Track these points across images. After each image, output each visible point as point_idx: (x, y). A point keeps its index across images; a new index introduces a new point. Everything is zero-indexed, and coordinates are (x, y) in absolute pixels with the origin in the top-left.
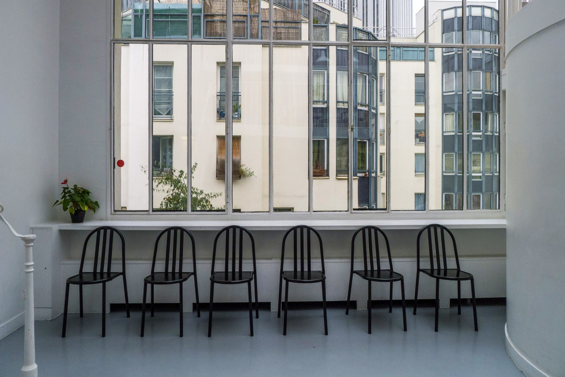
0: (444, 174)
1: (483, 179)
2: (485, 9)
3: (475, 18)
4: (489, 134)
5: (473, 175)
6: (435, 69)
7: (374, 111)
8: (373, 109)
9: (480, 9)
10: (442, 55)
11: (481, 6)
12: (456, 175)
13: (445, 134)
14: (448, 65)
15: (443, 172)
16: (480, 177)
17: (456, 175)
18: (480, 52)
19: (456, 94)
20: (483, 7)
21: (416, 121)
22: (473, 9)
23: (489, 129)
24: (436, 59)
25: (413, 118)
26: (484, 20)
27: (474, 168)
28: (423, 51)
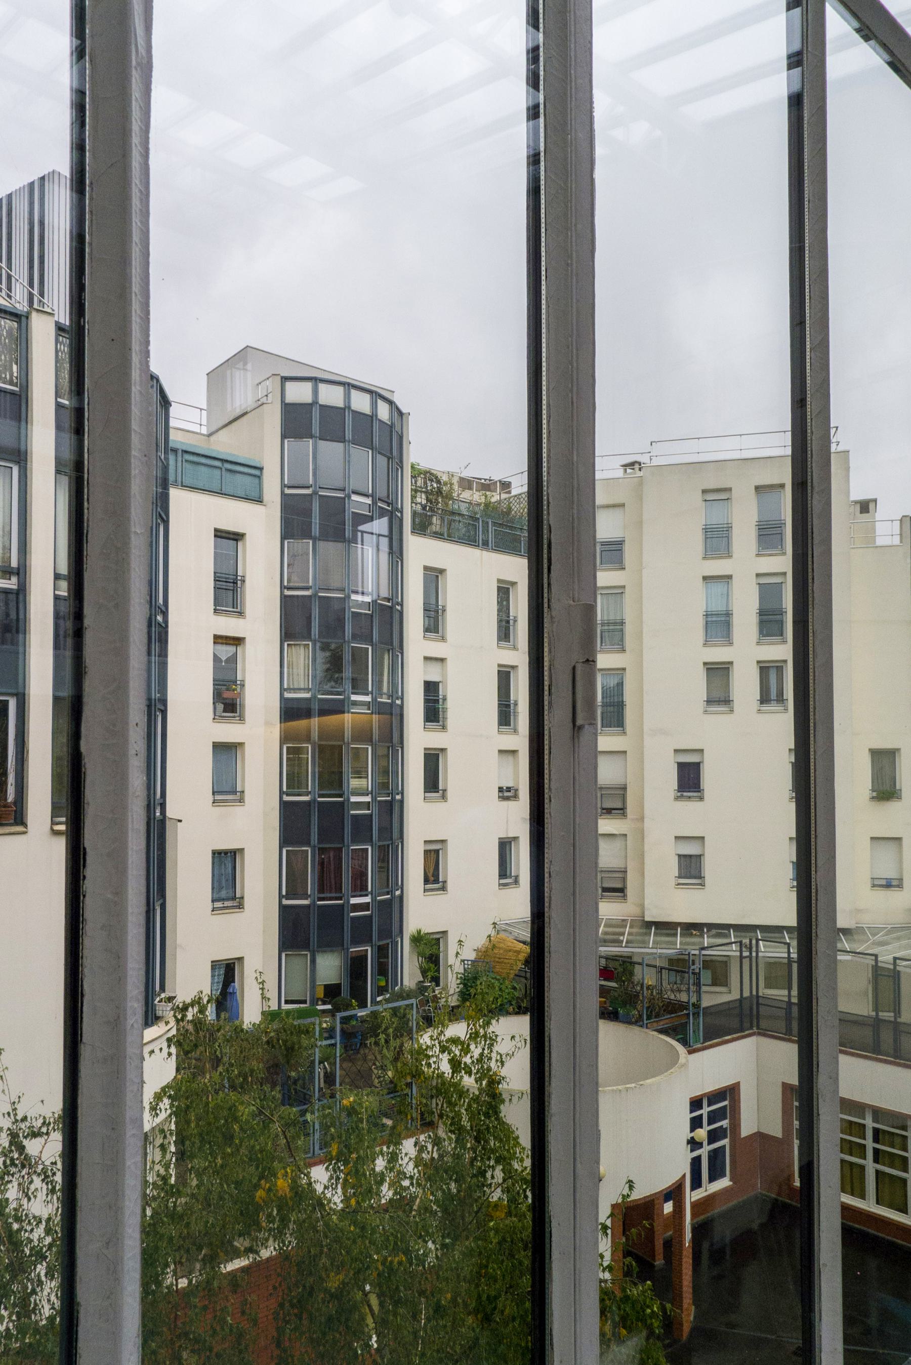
0: (286, 798)
1: (374, 811)
2: (354, 392)
3: (326, 409)
4: (384, 700)
5: (354, 799)
6: (261, 524)
7: (399, 608)
8: (398, 604)
9: (340, 389)
10: (282, 492)
11: (370, 392)
12: (314, 800)
13: (287, 695)
14: (296, 521)
15: (281, 793)
16: (367, 805)
17: (314, 800)
18: (369, 501)
19: (315, 595)
20: (349, 386)
21: (215, 656)
22: (322, 387)
23: (385, 690)
24: (266, 497)
25: (209, 648)
26: (376, 426)
27: (354, 783)
28: (233, 477)
